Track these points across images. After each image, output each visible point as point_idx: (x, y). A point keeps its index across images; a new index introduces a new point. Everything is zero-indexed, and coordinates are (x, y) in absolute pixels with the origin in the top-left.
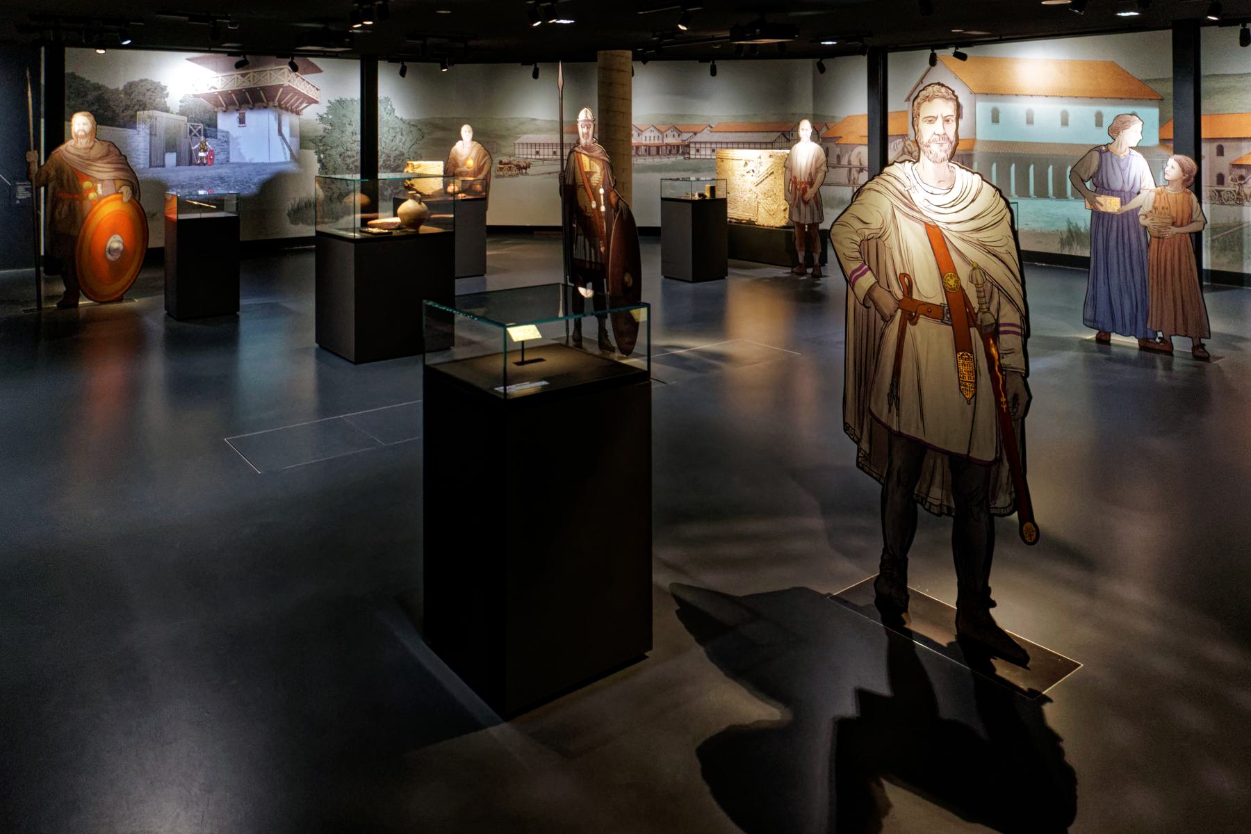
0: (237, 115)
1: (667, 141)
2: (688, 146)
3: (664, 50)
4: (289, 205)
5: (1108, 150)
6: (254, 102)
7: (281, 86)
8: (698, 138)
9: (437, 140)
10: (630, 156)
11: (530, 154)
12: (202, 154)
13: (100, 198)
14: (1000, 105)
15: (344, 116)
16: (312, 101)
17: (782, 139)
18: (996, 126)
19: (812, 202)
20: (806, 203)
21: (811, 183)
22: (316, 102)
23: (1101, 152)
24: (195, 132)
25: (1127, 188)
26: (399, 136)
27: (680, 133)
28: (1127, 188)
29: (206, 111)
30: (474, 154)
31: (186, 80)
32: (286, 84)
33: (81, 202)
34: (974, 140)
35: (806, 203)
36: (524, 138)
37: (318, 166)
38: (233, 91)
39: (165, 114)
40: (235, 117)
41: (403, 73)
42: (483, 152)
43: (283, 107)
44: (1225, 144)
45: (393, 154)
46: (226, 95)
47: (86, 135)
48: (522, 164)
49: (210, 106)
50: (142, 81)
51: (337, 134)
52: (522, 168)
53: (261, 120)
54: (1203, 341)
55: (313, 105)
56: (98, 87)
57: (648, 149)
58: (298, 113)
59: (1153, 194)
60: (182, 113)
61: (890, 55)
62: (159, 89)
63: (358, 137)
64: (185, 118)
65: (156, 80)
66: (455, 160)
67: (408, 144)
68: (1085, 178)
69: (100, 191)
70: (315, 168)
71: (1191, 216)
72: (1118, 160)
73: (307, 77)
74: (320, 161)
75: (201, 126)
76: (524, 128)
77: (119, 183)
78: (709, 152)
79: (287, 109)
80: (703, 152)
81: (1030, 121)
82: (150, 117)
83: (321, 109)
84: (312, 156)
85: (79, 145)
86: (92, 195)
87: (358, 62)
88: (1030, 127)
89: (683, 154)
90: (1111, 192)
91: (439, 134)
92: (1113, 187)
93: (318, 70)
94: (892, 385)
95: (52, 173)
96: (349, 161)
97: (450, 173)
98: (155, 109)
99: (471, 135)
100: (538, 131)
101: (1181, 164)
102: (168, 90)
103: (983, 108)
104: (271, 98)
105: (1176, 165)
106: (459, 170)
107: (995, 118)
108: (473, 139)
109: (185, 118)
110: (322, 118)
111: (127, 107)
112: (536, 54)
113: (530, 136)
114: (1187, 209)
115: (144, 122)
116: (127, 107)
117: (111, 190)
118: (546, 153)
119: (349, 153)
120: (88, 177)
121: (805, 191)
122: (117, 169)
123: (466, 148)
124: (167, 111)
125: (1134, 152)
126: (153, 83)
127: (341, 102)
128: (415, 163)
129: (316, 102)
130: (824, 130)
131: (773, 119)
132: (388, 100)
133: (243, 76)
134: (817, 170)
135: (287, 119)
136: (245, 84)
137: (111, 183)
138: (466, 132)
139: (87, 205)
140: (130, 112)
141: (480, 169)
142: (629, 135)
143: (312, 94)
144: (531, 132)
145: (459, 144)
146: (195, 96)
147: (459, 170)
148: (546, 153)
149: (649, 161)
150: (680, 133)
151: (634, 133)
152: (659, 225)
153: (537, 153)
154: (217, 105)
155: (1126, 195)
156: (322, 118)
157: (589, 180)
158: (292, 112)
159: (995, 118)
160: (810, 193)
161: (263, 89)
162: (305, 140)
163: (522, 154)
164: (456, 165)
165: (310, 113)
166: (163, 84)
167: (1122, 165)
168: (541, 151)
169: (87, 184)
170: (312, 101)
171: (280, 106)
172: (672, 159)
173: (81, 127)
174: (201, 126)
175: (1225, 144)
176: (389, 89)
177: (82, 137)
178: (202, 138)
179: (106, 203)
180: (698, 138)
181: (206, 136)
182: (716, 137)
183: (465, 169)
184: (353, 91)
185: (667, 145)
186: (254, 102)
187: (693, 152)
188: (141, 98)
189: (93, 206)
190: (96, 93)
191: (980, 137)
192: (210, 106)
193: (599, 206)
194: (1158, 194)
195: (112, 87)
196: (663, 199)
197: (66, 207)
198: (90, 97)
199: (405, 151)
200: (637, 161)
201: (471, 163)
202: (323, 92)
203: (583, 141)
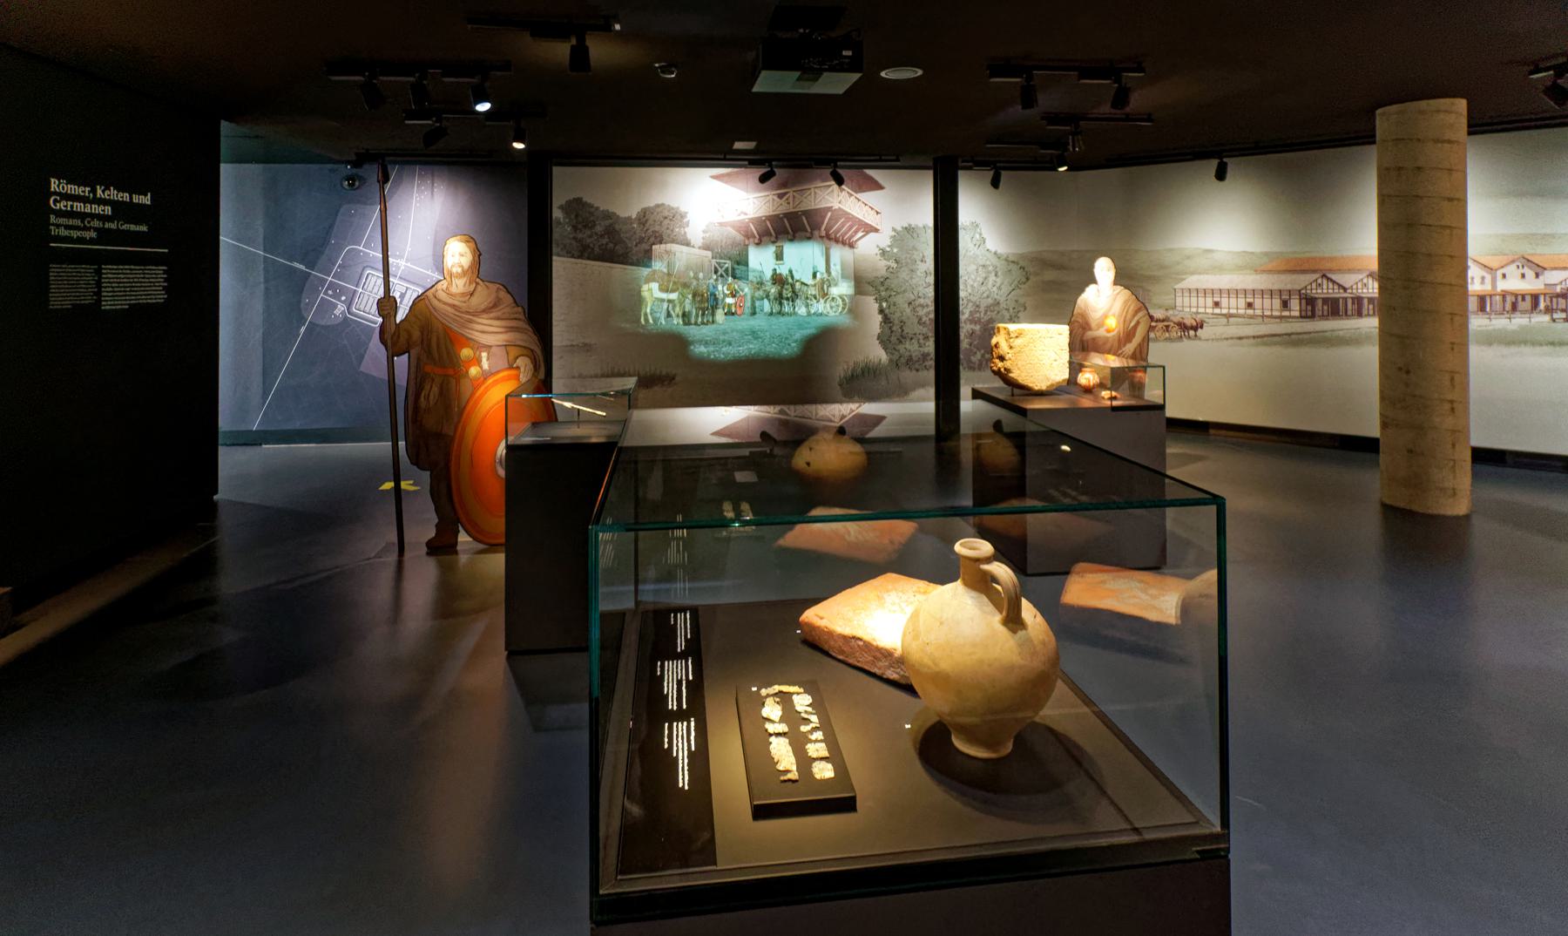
0: (772, 249)
1: (1502, 286)
4: (840, 370)
6: (795, 232)
7: (829, 209)
9: (1051, 287)
10: (1465, 316)
11: (1204, 307)
12: (730, 300)
13: (486, 376)
15: (914, 248)
16: (870, 229)
22: (876, 230)
24: (721, 271)
26: (992, 278)
27: (1539, 270)
29: (734, 244)
30: (1118, 306)
31: (710, 202)
32: (836, 206)
33: (458, 382)
36: (1192, 281)
37: (880, 318)
38: (769, 218)
39: (684, 248)
40: (771, 250)
41: (995, 183)
42: (1133, 306)
43: (830, 238)
45: (984, 304)
46: (759, 222)
47: (464, 273)
48: (1189, 322)
49: (739, 237)
50: (658, 206)
51: (904, 275)
52: (1190, 329)
53: (802, 259)
55: (872, 235)
56: (608, 215)
57: (1513, 303)
58: (851, 246)
60: (706, 247)
62: (675, 216)
63: (931, 279)
64: (709, 254)
65: (674, 204)
66: (1084, 316)
67: (1005, 289)
69: (485, 365)
70: (875, 322)
73: (864, 196)
74: (881, 311)
75: (728, 264)
77: (514, 352)
79: (837, 241)
82: (667, 252)
83: (883, 239)
84: (871, 305)
85: (454, 290)
86: (473, 371)
87: (929, 175)
91: (1050, 275)
93: (879, 187)
95: (416, 334)
96: (922, 312)
97: (1082, 345)
98: (673, 242)
99: (1111, 275)
100: (1219, 269)
102: (689, 217)
104: (816, 226)
106: (1090, 334)
108: (1116, 283)
109: (709, 254)
110: (883, 253)
111: (642, 240)
112: (1217, 140)
113: (1195, 277)
115: (661, 258)
116: (642, 240)
117: (503, 364)
118: (1236, 305)
119: (922, 301)
120: (468, 342)
122: (511, 329)
123: (1103, 299)
124: (688, 244)
126: (670, 209)
127: (909, 230)
128: (1012, 327)
129: (876, 230)
132: (975, 226)
133: (781, 196)
135: (838, 253)
136: (784, 208)
137: (500, 352)
138: (1104, 268)
139: (466, 388)
140: (645, 246)
141: (1129, 335)
143: (870, 219)
144: (1205, 272)
145: (1090, 290)
146: (721, 224)
147: (1090, 334)
148: (1236, 305)
149: (1501, 323)
150: (1539, 270)
151: (1474, 272)
153: (1217, 304)
154: (748, 235)
156: (883, 253)
158: (844, 243)
161: (807, 213)
162: (862, 283)
163: (1188, 307)
164: (1086, 326)
165: (869, 247)
166: (683, 209)
168: (1224, 302)
169: (466, 353)
170: (870, 229)
171: (828, 237)
172: (1519, 321)
173: (457, 259)
174: (728, 264)
176: (977, 214)
177: (459, 276)
178: (730, 279)
179: (496, 383)
181: (734, 277)
183: (1101, 332)
184: (923, 214)
185: (1504, 295)
186: (795, 232)
187: (720, 315)
188: (657, 228)
189: (476, 388)
190: (607, 222)
192: (739, 237)
195: (623, 214)
197: (435, 389)
198: (598, 229)
199: (1002, 300)
200: (1477, 323)
201: (1112, 323)
202: (885, 215)
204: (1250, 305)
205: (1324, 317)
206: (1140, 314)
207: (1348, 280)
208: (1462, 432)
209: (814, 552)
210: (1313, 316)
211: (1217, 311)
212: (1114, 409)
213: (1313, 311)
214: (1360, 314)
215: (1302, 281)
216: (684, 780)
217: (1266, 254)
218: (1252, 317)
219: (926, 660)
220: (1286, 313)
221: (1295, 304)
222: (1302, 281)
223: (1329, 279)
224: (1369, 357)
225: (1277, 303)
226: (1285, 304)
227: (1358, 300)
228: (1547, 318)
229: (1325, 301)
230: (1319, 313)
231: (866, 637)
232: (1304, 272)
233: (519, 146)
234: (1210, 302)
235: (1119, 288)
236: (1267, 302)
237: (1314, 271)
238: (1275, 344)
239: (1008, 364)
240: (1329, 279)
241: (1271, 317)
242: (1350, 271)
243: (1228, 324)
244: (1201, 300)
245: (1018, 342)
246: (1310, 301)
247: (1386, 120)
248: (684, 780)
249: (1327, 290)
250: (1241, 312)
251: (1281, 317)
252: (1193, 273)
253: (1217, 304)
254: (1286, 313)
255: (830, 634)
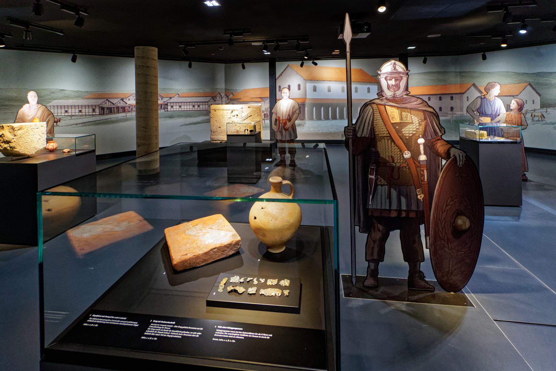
2: (167, 105)
3: (169, 55)
5: (485, 98)
8: (172, 100)
10: (157, 110)
14: (317, 85)
17: (213, 100)
18: (315, 92)
19: (290, 129)
20: (286, 130)
21: (289, 120)
23: (481, 98)
25: (494, 113)
28: (494, 113)
34: (306, 98)
35: (286, 130)
44: (454, 96)
54: (525, 173)
59: (505, 115)
61: (409, 58)
68: (474, 110)
71: (521, 123)
72: (490, 101)
76: (54, 95)
78: (178, 107)
80: (175, 107)
81: (329, 90)
88: (329, 93)
89: (164, 108)
90: (486, 115)
92: (487, 113)
94: (56, 193)
99: (36, 99)
100: (67, 97)
101: (517, 102)
103: (309, 86)
105: (515, 103)
107: (315, 89)
108: (38, 103)
113: (56, 101)
114: (520, 121)
118: (75, 111)
121: (285, 124)
125: (497, 98)
130: (231, 96)
131: (208, 90)
134: (293, 113)
142: (158, 99)
145: (26, 106)
148: (75, 111)
152: (135, 149)
153: (66, 112)
155: (493, 117)
157: (398, 132)
159: (315, 89)
160: (289, 124)
166: (487, 57)
167: (492, 104)
175: (454, 96)
180: (172, 100)
182: (181, 100)
187: (169, 107)
191: (308, 97)
193: (415, 154)
194: (508, 115)
196: (228, 135)
203: (388, 93)
204: (80, 111)
205: (107, 114)
206: (50, 116)
207: (115, 101)
208: (157, 144)
209: (111, 244)
210: (104, 114)
211: (67, 114)
212: (77, 155)
213: (104, 112)
214: (118, 112)
215: (99, 102)
216: (267, 336)
217: (87, 92)
218: (81, 116)
219: (285, 223)
220: (94, 114)
221: (97, 110)
222: (99, 102)
223: (109, 101)
224: (132, 124)
225: (91, 110)
226: (94, 110)
227: (118, 108)
228: (164, 111)
229: (107, 108)
230: (105, 113)
231: (217, 246)
232: (101, 98)
233: (523, 32)
234: (63, 111)
235: (40, 105)
236: (87, 110)
237: (104, 98)
238: (90, 125)
239: (12, 145)
240: (109, 101)
241: (89, 115)
242: (115, 98)
243: (71, 119)
244: (59, 110)
245: (19, 133)
246: (103, 109)
247: (137, 50)
248: (267, 336)
249: (108, 105)
250: (77, 114)
251: (93, 115)
252: (55, 99)
253: (66, 112)
254: (94, 114)
255: (197, 257)
